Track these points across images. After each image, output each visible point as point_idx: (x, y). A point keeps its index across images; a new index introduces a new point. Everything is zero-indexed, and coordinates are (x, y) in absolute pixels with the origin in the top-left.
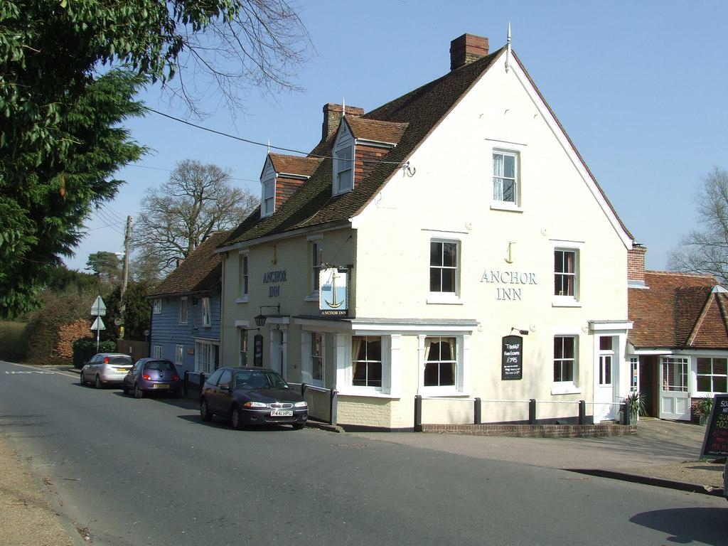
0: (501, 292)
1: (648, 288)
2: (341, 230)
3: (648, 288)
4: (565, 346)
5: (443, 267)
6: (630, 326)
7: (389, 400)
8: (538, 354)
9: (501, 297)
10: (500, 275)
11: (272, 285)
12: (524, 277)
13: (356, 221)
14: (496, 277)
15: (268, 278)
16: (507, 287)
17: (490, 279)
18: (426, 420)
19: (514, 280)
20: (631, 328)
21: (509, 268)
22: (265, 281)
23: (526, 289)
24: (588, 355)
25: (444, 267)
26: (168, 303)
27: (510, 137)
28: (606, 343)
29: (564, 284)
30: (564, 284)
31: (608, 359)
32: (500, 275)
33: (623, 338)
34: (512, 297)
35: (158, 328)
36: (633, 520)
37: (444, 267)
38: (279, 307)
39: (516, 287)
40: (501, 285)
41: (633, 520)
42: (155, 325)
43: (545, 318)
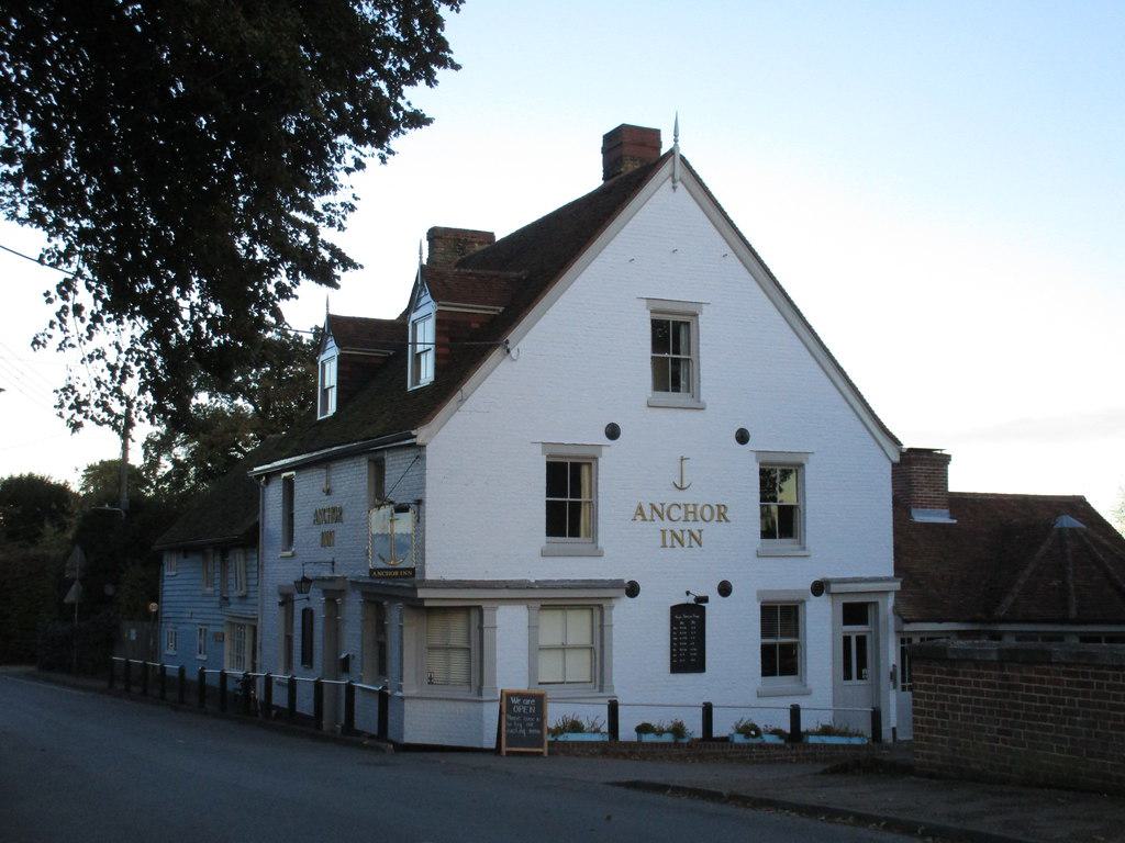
0: (668, 535)
1: (955, 521)
2: (410, 446)
3: (955, 521)
4: (780, 617)
5: (569, 499)
6: (897, 585)
7: (482, 701)
8: (734, 636)
9: (669, 543)
10: (665, 509)
11: (327, 528)
12: (707, 510)
13: (421, 435)
14: (659, 512)
15: (319, 517)
16: (678, 527)
17: (648, 514)
18: (586, 641)
19: (691, 517)
20: (899, 588)
21: (682, 497)
22: (317, 521)
23: (712, 531)
24: (821, 630)
25: (567, 494)
26: (185, 557)
27: (676, 291)
28: (855, 613)
29: (782, 524)
30: (782, 524)
31: (861, 641)
32: (665, 509)
33: (888, 604)
34: (687, 535)
35: (171, 583)
36: (428, 121)
37: (567, 494)
38: (333, 563)
39: (694, 527)
40: (667, 524)
41: (428, 121)
42: (168, 588)
43: (740, 569)
